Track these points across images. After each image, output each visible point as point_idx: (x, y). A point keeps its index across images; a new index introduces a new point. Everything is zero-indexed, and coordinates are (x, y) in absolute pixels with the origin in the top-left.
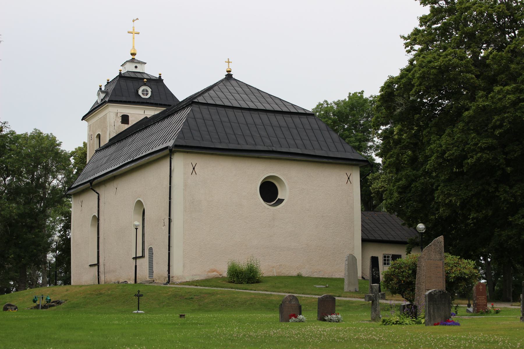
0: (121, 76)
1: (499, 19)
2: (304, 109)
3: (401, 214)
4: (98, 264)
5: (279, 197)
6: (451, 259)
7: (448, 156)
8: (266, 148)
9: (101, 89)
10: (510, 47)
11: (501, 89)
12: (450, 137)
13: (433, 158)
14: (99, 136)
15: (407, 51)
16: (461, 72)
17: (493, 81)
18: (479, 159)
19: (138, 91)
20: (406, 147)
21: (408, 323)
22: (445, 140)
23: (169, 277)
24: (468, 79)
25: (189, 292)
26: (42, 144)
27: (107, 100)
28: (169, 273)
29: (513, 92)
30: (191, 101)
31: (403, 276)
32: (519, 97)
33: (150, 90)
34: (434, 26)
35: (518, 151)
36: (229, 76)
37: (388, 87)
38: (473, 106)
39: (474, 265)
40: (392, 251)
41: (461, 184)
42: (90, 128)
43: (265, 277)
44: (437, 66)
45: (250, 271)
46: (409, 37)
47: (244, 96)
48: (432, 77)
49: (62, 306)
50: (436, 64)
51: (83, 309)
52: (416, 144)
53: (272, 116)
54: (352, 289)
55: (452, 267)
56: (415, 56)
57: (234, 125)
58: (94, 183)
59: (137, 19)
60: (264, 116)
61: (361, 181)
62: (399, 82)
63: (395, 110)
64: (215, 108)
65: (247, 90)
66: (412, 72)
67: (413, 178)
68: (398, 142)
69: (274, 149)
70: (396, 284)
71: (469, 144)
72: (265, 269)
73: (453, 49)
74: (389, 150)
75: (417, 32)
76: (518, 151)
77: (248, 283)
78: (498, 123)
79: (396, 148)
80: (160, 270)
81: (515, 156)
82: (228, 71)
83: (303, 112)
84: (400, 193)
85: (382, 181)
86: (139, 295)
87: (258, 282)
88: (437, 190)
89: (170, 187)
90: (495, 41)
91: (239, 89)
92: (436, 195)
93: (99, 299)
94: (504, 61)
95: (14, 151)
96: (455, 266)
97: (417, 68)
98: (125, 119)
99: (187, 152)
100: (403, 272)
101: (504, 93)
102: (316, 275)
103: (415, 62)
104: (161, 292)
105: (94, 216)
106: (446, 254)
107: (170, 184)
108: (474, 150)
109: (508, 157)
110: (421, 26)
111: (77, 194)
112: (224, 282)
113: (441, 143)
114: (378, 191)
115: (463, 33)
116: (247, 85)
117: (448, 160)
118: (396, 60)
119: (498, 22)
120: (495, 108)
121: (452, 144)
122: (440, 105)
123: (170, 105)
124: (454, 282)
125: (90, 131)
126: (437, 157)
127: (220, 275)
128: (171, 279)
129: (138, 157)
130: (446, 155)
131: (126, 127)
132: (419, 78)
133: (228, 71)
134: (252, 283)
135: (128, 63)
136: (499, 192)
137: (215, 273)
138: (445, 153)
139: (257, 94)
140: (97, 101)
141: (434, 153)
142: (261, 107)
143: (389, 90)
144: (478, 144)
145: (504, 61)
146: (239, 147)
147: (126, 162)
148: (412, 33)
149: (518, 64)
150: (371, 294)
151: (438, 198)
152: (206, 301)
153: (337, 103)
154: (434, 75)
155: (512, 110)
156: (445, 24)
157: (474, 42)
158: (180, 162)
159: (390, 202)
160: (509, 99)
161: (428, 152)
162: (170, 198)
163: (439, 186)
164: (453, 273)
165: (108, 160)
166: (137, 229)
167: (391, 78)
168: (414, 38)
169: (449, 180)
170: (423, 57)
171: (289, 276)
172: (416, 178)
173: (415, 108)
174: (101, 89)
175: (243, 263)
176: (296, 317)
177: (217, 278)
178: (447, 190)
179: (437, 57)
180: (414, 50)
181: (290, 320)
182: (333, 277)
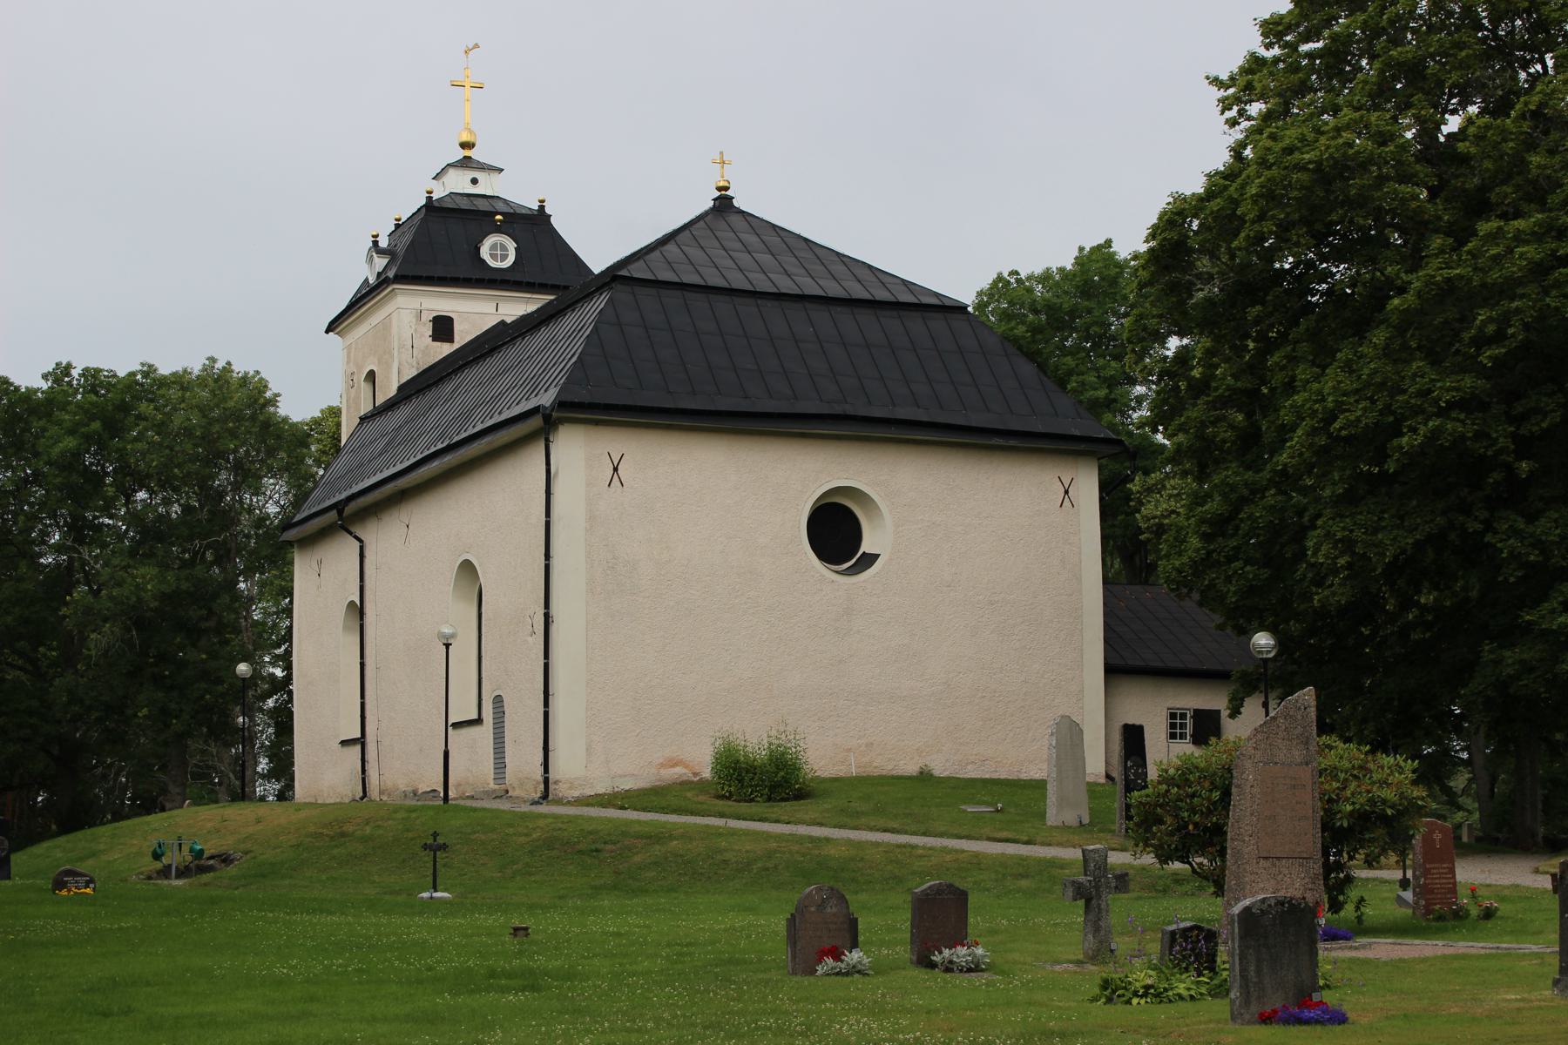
0: (432, 209)
1: (1495, 21)
2: (937, 295)
3: (1211, 598)
4: (361, 741)
5: (866, 547)
6: (1344, 753)
7: (1342, 428)
8: (825, 410)
9: (375, 243)
10: (1526, 104)
11: (1500, 228)
12: (1351, 372)
13: (1300, 432)
14: (371, 376)
15: (1227, 121)
16: (1382, 180)
17: (1479, 206)
18: (1435, 434)
20: (1225, 402)
21: (1185, 993)
22: (1333, 380)
23: (546, 781)
24: (1403, 201)
25: (590, 833)
26: (225, 400)
27: (391, 274)
28: (546, 770)
29: (1537, 237)
30: (615, 276)
31: (1193, 811)
32: (1554, 251)
33: (511, 246)
34: (1305, 48)
35: (1553, 411)
36: (724, 204)
37: (1171, 224)
38: (1416, 282)
39: (1414, 771)
40: (1194, 699)
41: (1383, 512)
43: (824, 780)
45: (777, 766)
46: (1232, 78)
47: (765, 258)
48: (1295, 194)
49: (232, 870)
50: (1307, 156)
51: (287, 882)
52: (1254, 393)
54: (1070, 818)
55: (1346, 780)
56: (1250, 132)
57: (736, 340)
58: (348, 510)
59: (476, 46)
60: (820, 315)
61: (1101, 499)
62: (1202, 209)
63: (1191, 296)
64: (678, 293)
65: (774, 240)
66: (1239, 181)
67: (1246, 492)
68: (1200, 388)
69: (850, 410)
70: (1171, 834)
71: (1404, 392)
72: (822, 758)
73: (1357, 109)
74: (1176, 411)
75: (1255, 64)
76: (1553, 411)
77: (769, 799)
78: (1491, 328)
79: (1195, 405)
80: (524, 760)
81: (1544, 425)
82: (719, 189)
83: (934, 301)
84: (1206, 538)
85: (1170, 496)
86: (435, 847)
87: (801, 794)
88: (1315, 528)
89: (548, 524)
90: (1484, 85)
91: (751, 239)
92: (1310, 544)
93: (335, 851)
94: (1511, 144)
96: (1355, 777)
97: (1252, 170)
98: (442, 328)
99: (597, 423)
100: (1193, 796)
101: (1509, 242)
102: (972, 772)
103: (1248, 152)
104: (511, 831)
105: (352, 603)
106: (1325, 739)
107: (548, 514)
108: (1417, 411)
109: (1523, 431)
110: (1268, 47)
111: (311, 541)
112: (702, 798)
113: (1325, 391)
114: (1160, 525)
115: (1387, 65)
116: (774, 226)
117: (1348, 440)
118: (1196, 147)
119: (1494, 31)
120: (1484, 285)
121: (1357, 391)
122: (1325, 276)
123: (566, 288)
124: (1350, 829)
126: (1314, 431)
127: (695, 774)
128: (551, 787)
129: (464, 435)
130: (1337, 425)
131: (445, 349)
132: (1255, 199)
134: (783, 800)
135: (452, 171)
136: (1496, 533)
137: (679, 770)
138: (1335, 419)
140: (367, 280)
141: (1303, 419)
142: (812, 289)
143: (1173, 235)
144: (1430, 391)
145: (1511, 144)
146: (744, 406)
147: (433, 449)
148: (1241, 68)
149: (1551, 152)
150: (1082, 879)
151: (1315, 554)
152: (637, 859)
153: (1045, 278)
154: (1303, 188)
155: (1532, 289)
156: (1334, 38)
157: (1422, 90)
158: (577, 453)
159: (1177, 563)
160: (1520, 257)
161: (1286, 416)
162: (547, 556)
163: (1319, 516)
164: (1347, 799)
165: (387, 444)
166: (447, 646)
167: (1179, 199)
168: (1247, 82)
169: (1349, 499)
170: (1273, 137)
171: (893, 777)
172: (1256, 491)
173: (1252, 285)
174: (375, 243)
175: (755, 739)
176: (837, 958)
177: (684, 784)
178: (1344, 529)
179: (1311, 136)
180: (1249, 118)
181: (819, 968)
182: (1024, 776)
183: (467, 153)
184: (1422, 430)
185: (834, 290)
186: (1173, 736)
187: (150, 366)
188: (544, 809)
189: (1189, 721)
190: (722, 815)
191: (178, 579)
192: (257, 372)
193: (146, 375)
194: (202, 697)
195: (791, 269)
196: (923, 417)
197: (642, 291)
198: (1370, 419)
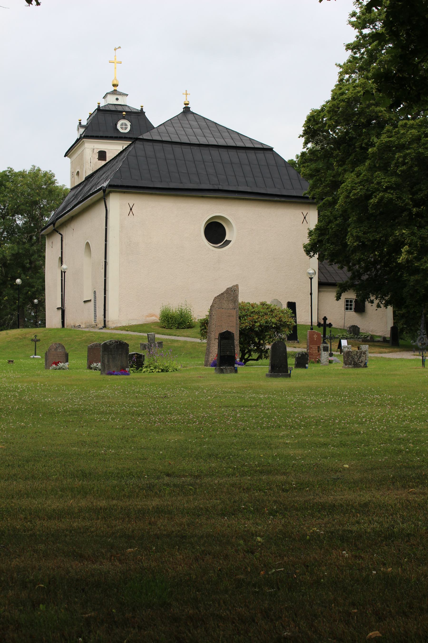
0: (99, 110)
2: (262, 144)
5: (227, 238)
8: (211, 187)
9: (80, 123)
18: (382, 198)
19: (116, 125)
28: (105, 317)
33: (129, 124)
36: (187, 110)
42: (72, 165)
44: (346, 99)
47: (198, 131)
53: (224, 152)
58: (57, 224)
59: (120, 47)
60: (215, 152)
65: (203, 124)
69: (221, 188)
71: (373, 183)
78: (401, 160)
82: (185, 104)
83: (260, 146)
91: (194, 123)
95: (8, 188)
98: (102, 155)
99: (124, 192)
108: (378, 190)
116: (204, 118)
125: (72, 168)
131: (103, 163)
133: (185, 104)
134: (183, 328)
139: (214, 129)
142: (213, 142)
158: (117, 204)
162: (106, 241)
167: (314, 111)
174: (80, 123)
175: (175, 306)
176: (56, 365)
183: (115, 88)
184: (378, 197)
185: (221, 142)
186: (347, 309)
187: (11, 169)
188: (104, 331)
189: (353, 303)
190: (163, 334)
191: (19, 249)
192: (50, 171)
193: (10, 172)
194: (28, 292)
195: (206, 135)
196: (249, 190)
197: (146, 143)
198: (362, 193)
